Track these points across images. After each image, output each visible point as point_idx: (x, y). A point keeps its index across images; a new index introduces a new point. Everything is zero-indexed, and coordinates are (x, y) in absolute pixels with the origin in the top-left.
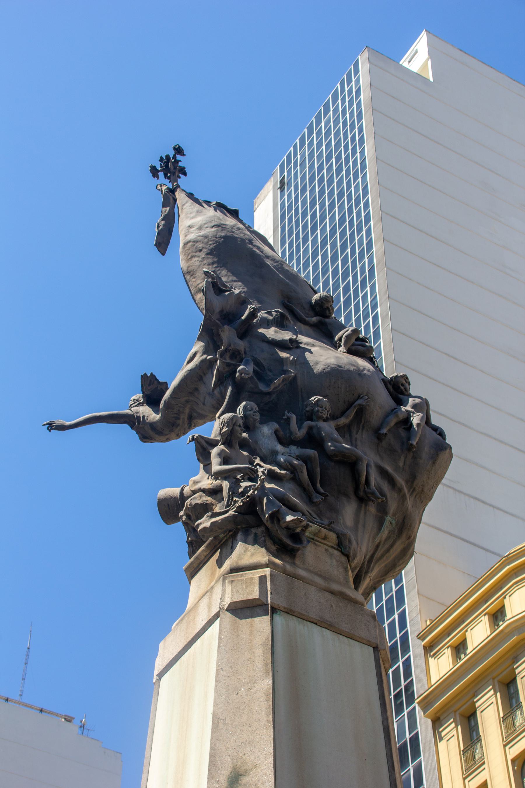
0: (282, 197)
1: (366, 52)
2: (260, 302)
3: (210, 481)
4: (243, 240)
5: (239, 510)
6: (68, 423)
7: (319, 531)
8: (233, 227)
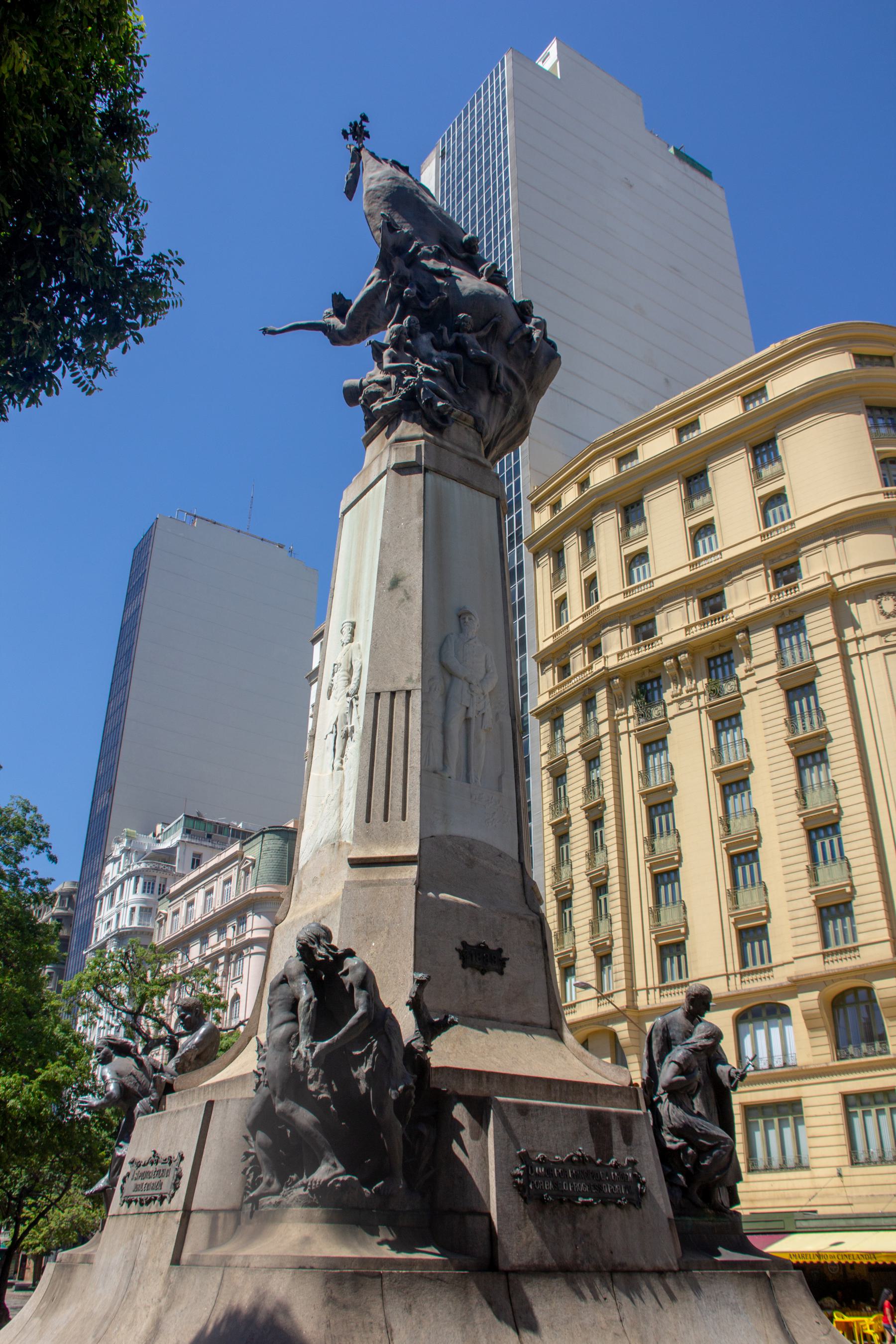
0: (443, 163)
1: (510, 52)
2: (423, 239)
3: (382, 375)
4: (411, 191)
5: (403, 397)
6: (277, 329)
7: (461, 415)
8: (404, 180)
